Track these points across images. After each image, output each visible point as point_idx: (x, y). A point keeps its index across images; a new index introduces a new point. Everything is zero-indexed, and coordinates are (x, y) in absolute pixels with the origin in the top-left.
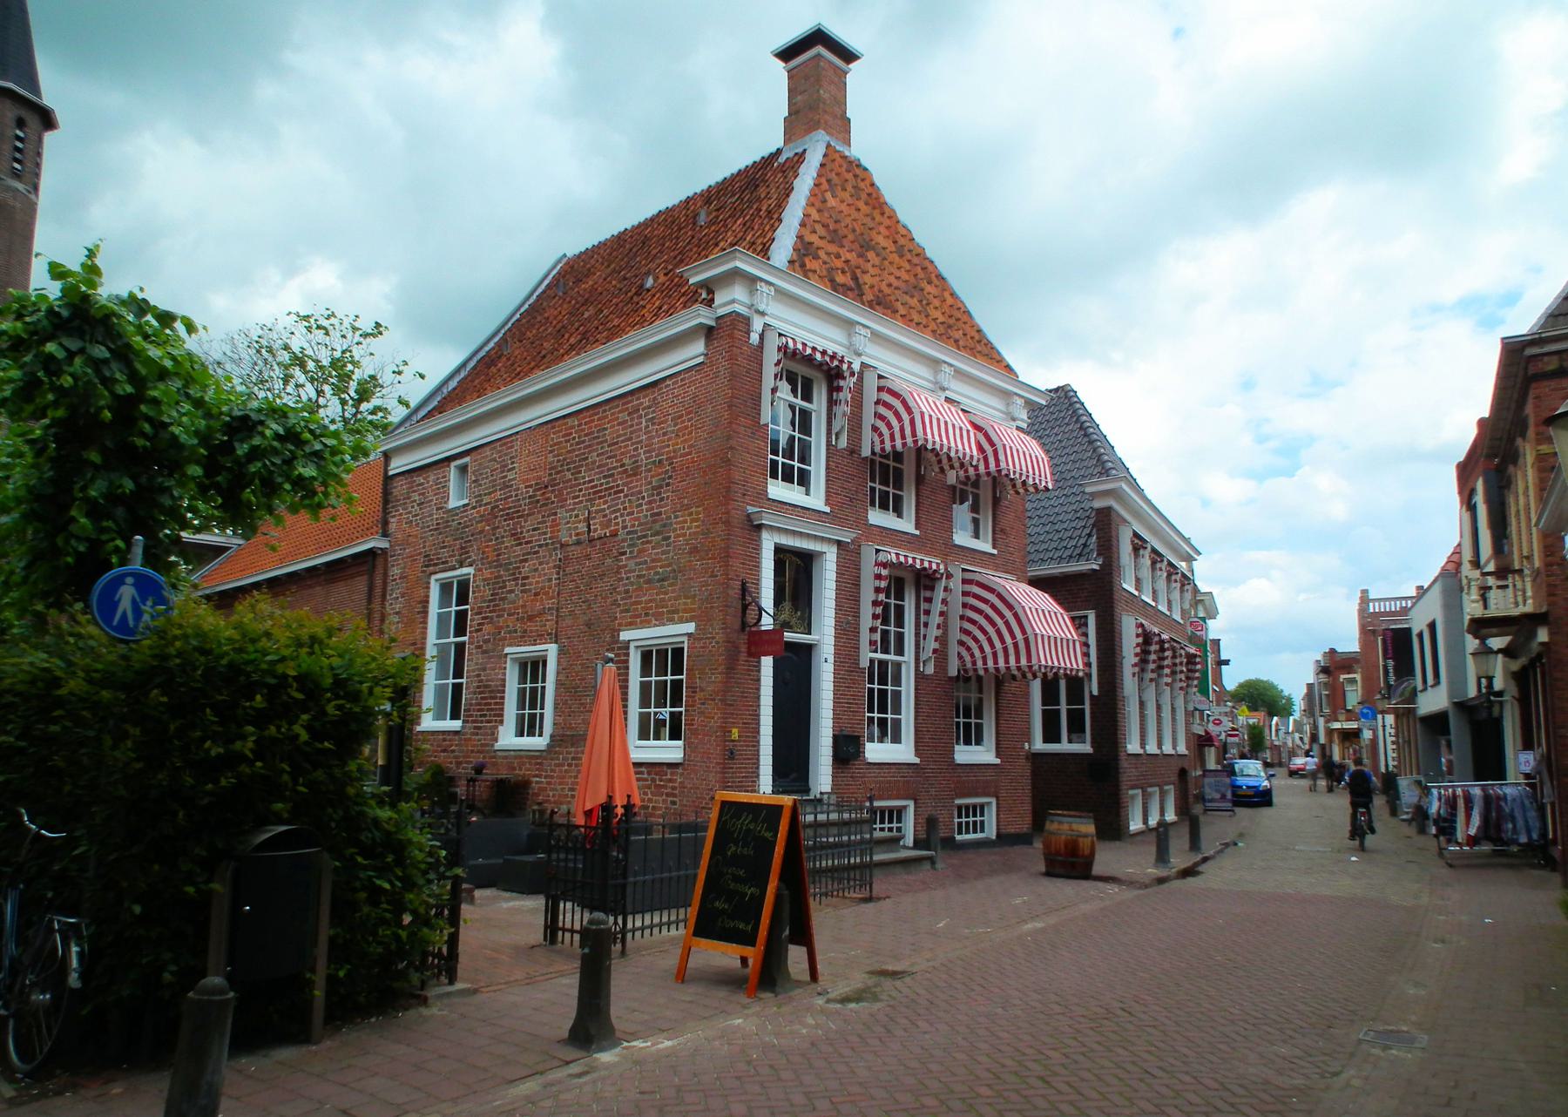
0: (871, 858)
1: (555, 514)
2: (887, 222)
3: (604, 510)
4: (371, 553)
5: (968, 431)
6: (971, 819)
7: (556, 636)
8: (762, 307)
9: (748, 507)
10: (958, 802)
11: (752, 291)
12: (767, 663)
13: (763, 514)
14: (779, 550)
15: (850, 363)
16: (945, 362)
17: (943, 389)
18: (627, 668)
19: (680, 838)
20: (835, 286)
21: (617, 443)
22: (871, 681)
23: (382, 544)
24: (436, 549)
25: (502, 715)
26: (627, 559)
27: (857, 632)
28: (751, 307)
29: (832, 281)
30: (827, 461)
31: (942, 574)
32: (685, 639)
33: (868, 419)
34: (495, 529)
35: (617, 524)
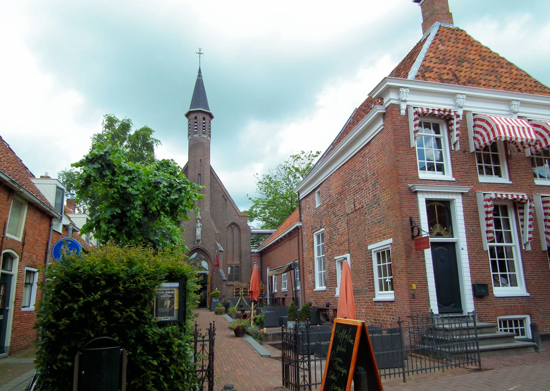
0: (478, 347)
1: (344, 203)
2: (475, 48)
3: (358, 198)
4: (297, 228)
5: (528, 128)
8: (403, 99)
9: (409, 185)
11: (399, 93)
12: (428, 253)
13: (416, 186)
14: (428, 201)
15: (455, 112)
17: (516, 113)
18: (372, 261)
19: (392, 335)
20: (442, 80)
21: (360, 170)
23: (300, 224)
26: (368, 216)
28: (399, 100)
30: (451, 158)
31: (527, 200)
32: (389, 246)
33: (471, 134)
34: (328, 213)
35: (363, 202)
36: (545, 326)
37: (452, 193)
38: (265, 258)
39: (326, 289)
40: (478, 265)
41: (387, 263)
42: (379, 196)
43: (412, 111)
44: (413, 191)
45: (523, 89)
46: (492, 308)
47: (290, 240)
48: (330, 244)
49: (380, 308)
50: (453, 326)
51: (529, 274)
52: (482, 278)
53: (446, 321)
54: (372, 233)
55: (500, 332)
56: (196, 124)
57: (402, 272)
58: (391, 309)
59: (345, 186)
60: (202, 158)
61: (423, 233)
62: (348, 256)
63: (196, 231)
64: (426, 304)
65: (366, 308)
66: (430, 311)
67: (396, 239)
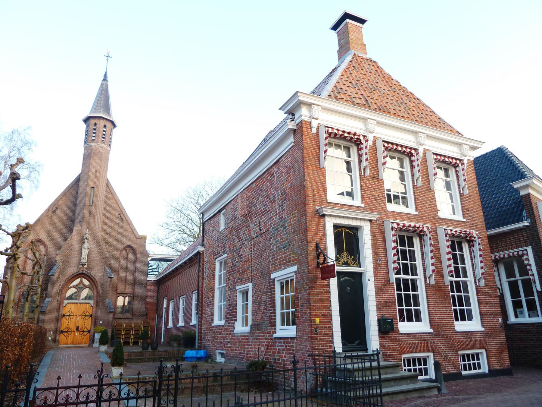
3: (264, 220)
4: (198, 253)
6: (471, 362)
7: (251, 279)
9: (317, 207)
10: (461, 352)
11: (310, 110)
12: (334, 282)
14: (336, 227)
16: (420, 132)
18: (274, 291)
22: (453, 291)
24: (217, 248)
25: (236, 317)
27: (387, 264)
29: (353, 102)
34: (232, 237)
35: (269, 225)
36: (447, 365)
37: (361, 219)
38: (162, 287)
39: (225, 323)
40: (384, 298)
41: (290, 294)
42: (285, 218)
43: (322, 130)
44: (321, 214)
45: (429, 124)
46: (397, 346)
47: (191, 267)
48: (232, 272)
49: (281, 346)
50: (356, 366)
51: (433, 309)
52: (387, 313)
53: (349, 361)
54: (276, 260)
55: (404, 371)
56: (94, 131)
57: (306, 304)
58: (292, 346)
59: (251, 207)
60: (98, 170)
61: (329, 260)
62: (250, 285)
63: (81, 252)
64: (329, 341)
65: (266, 345)
66: (333, 349)
67: (301, 266)
